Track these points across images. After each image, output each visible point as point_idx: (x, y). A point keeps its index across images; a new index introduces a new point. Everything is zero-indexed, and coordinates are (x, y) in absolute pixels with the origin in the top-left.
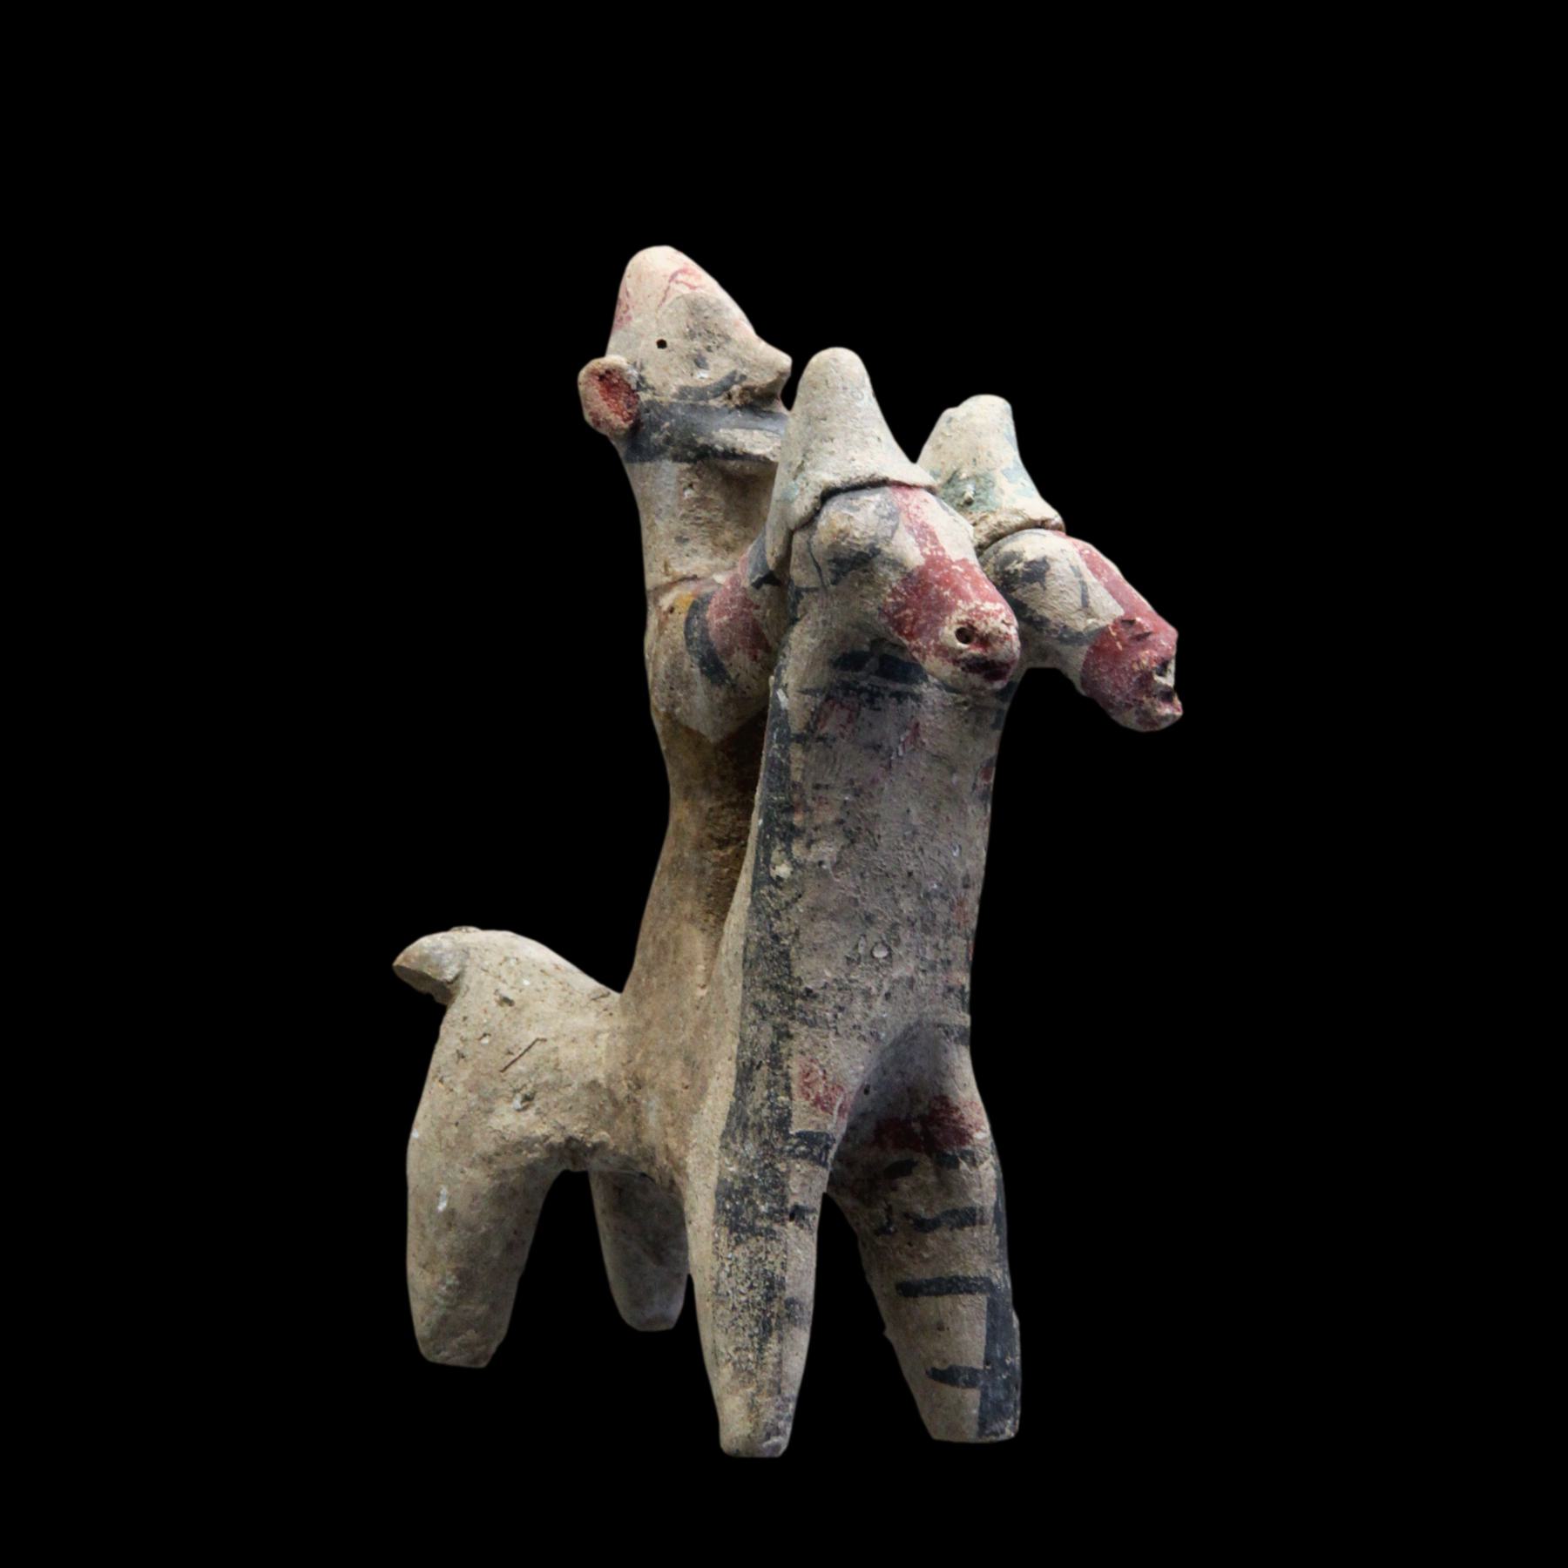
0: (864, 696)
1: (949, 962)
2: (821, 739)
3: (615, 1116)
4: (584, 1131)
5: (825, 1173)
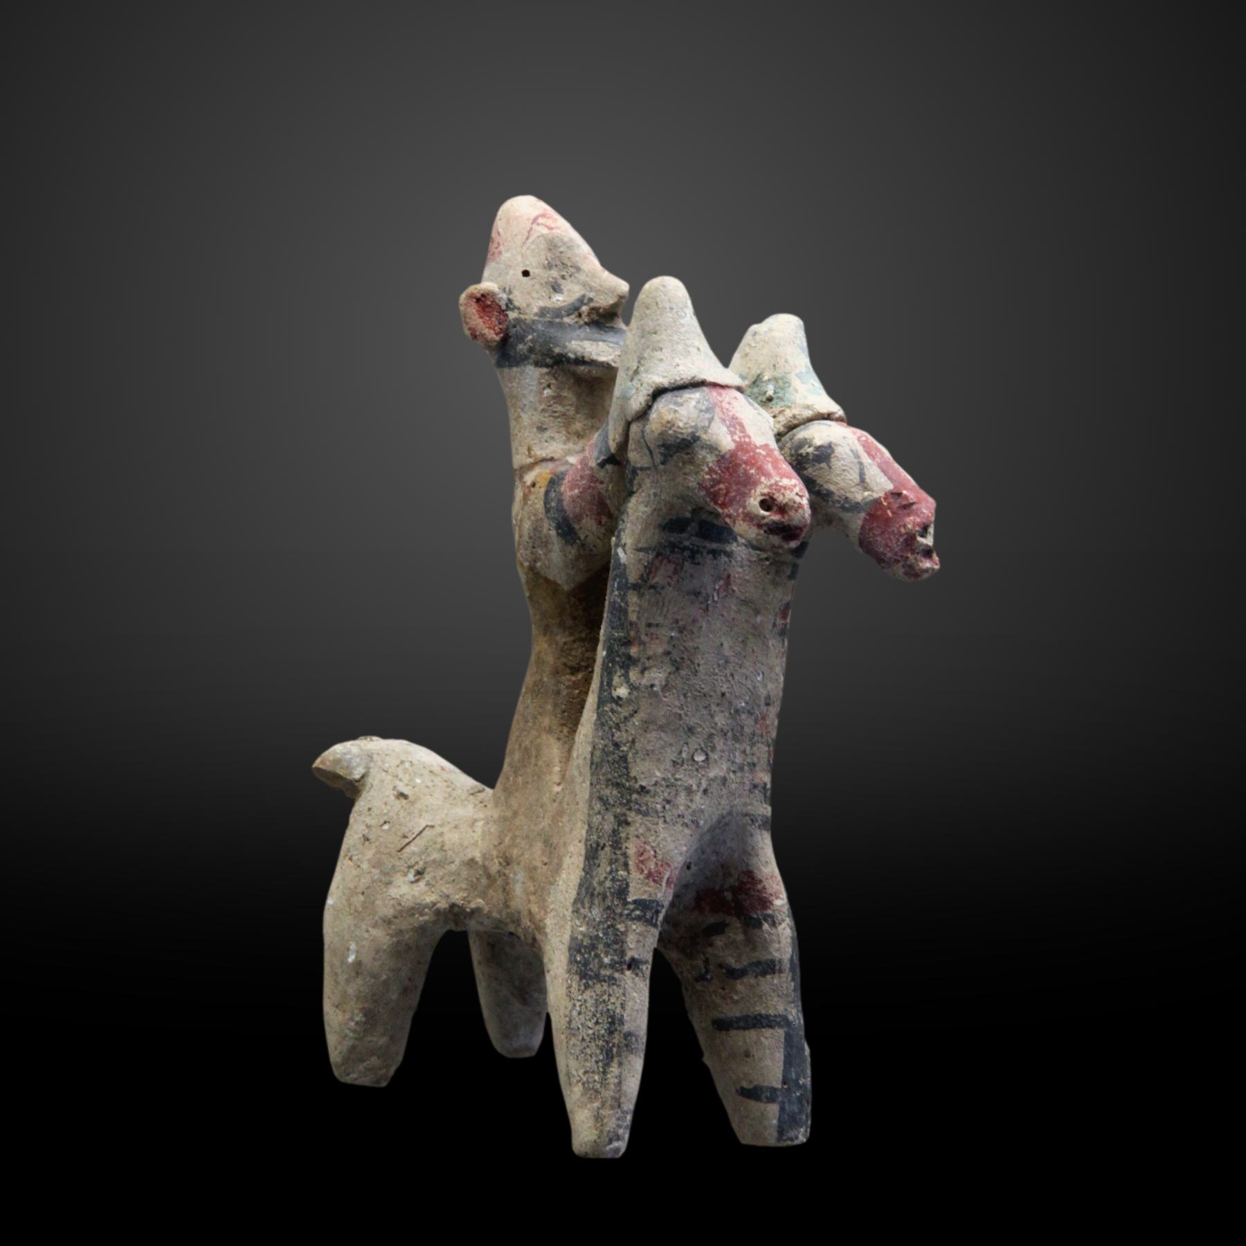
0: (687, 553)
1: (754, 765)
2: (652, 587)
3: (489, 886)
4: (464, 899)
5: (655, 932)
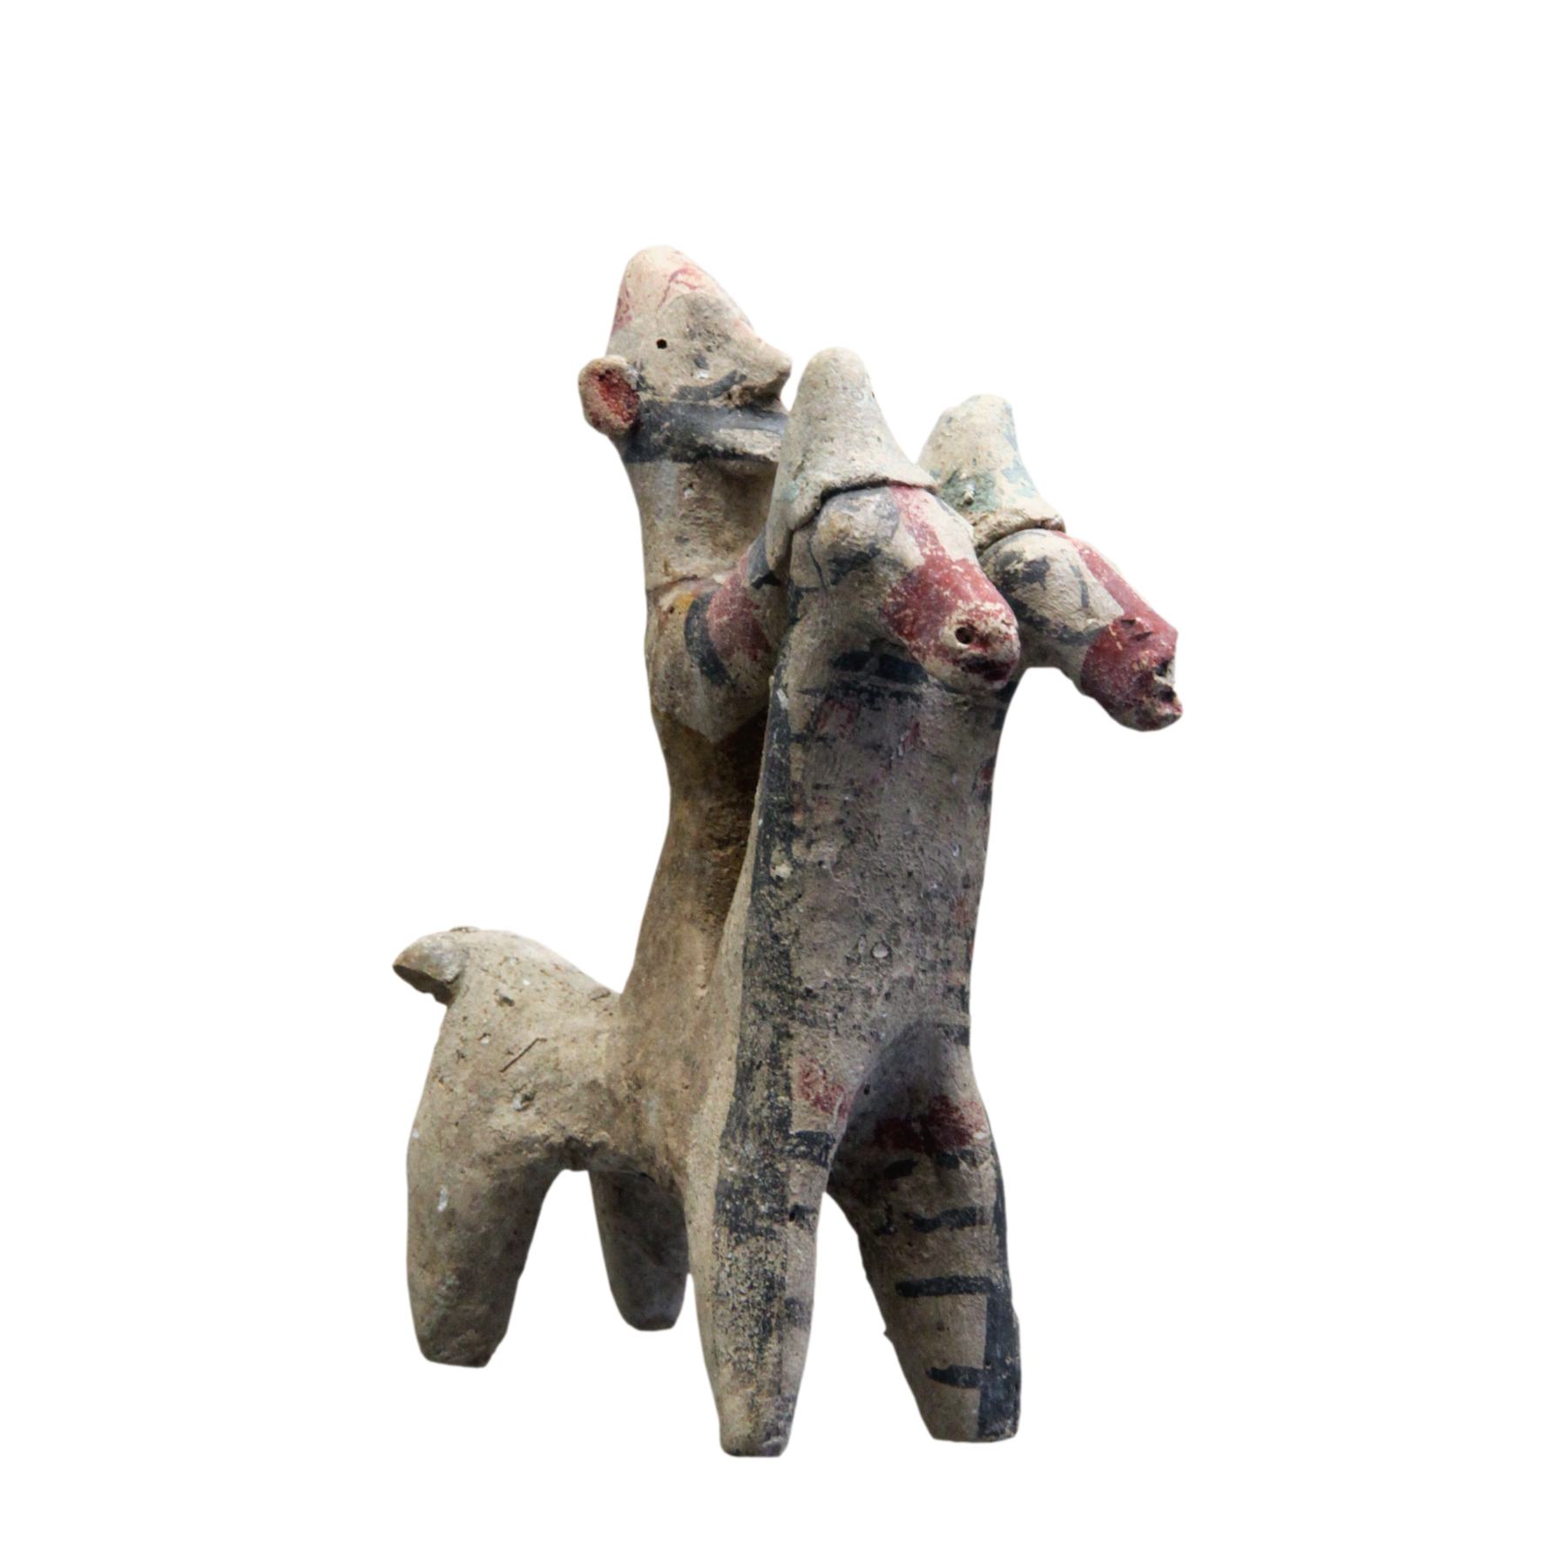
0: (864, 696)
1: (949, 962)
2: (821, 739)
3: (615, 1116)
4: (584, 1131)
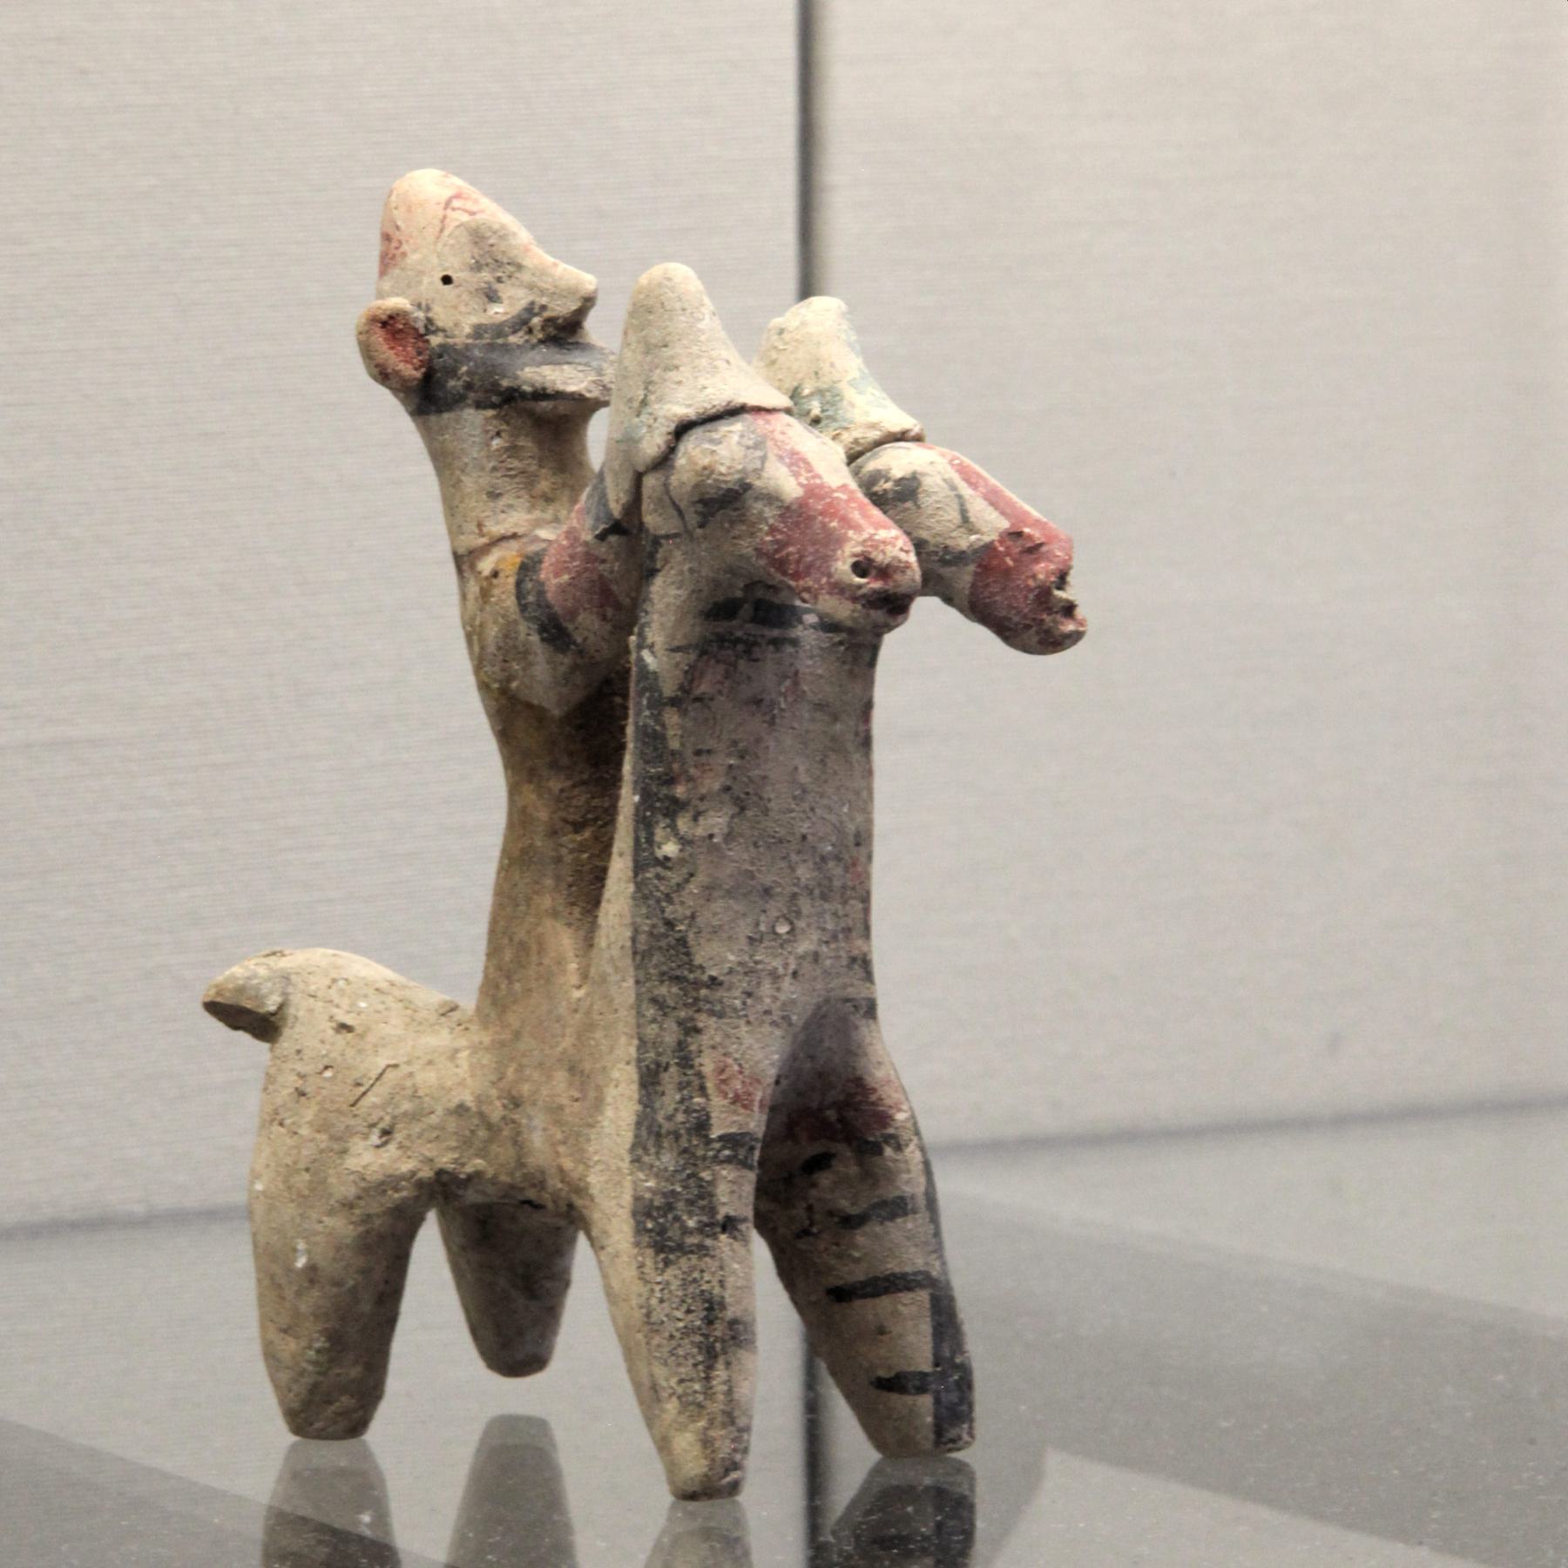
0: (740, 647)
2: (698, 699)
3: (490, 1141)
4: (455, 1161)
5: (751, 1176)
